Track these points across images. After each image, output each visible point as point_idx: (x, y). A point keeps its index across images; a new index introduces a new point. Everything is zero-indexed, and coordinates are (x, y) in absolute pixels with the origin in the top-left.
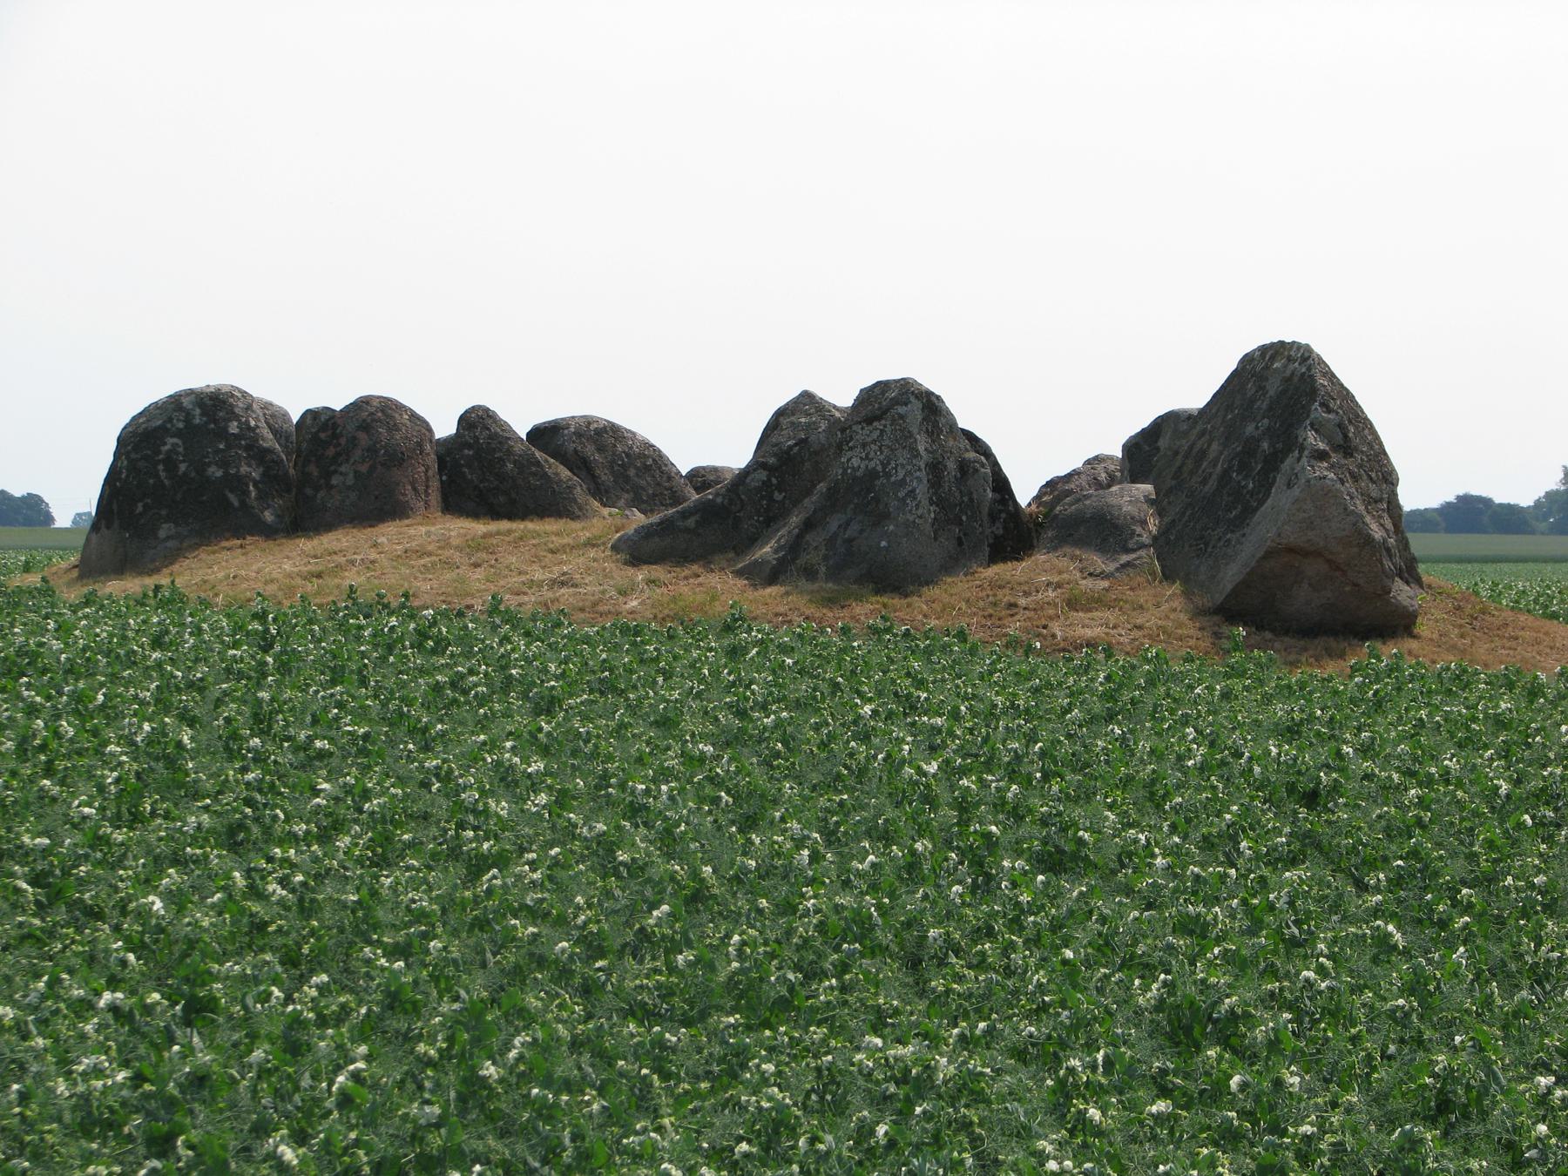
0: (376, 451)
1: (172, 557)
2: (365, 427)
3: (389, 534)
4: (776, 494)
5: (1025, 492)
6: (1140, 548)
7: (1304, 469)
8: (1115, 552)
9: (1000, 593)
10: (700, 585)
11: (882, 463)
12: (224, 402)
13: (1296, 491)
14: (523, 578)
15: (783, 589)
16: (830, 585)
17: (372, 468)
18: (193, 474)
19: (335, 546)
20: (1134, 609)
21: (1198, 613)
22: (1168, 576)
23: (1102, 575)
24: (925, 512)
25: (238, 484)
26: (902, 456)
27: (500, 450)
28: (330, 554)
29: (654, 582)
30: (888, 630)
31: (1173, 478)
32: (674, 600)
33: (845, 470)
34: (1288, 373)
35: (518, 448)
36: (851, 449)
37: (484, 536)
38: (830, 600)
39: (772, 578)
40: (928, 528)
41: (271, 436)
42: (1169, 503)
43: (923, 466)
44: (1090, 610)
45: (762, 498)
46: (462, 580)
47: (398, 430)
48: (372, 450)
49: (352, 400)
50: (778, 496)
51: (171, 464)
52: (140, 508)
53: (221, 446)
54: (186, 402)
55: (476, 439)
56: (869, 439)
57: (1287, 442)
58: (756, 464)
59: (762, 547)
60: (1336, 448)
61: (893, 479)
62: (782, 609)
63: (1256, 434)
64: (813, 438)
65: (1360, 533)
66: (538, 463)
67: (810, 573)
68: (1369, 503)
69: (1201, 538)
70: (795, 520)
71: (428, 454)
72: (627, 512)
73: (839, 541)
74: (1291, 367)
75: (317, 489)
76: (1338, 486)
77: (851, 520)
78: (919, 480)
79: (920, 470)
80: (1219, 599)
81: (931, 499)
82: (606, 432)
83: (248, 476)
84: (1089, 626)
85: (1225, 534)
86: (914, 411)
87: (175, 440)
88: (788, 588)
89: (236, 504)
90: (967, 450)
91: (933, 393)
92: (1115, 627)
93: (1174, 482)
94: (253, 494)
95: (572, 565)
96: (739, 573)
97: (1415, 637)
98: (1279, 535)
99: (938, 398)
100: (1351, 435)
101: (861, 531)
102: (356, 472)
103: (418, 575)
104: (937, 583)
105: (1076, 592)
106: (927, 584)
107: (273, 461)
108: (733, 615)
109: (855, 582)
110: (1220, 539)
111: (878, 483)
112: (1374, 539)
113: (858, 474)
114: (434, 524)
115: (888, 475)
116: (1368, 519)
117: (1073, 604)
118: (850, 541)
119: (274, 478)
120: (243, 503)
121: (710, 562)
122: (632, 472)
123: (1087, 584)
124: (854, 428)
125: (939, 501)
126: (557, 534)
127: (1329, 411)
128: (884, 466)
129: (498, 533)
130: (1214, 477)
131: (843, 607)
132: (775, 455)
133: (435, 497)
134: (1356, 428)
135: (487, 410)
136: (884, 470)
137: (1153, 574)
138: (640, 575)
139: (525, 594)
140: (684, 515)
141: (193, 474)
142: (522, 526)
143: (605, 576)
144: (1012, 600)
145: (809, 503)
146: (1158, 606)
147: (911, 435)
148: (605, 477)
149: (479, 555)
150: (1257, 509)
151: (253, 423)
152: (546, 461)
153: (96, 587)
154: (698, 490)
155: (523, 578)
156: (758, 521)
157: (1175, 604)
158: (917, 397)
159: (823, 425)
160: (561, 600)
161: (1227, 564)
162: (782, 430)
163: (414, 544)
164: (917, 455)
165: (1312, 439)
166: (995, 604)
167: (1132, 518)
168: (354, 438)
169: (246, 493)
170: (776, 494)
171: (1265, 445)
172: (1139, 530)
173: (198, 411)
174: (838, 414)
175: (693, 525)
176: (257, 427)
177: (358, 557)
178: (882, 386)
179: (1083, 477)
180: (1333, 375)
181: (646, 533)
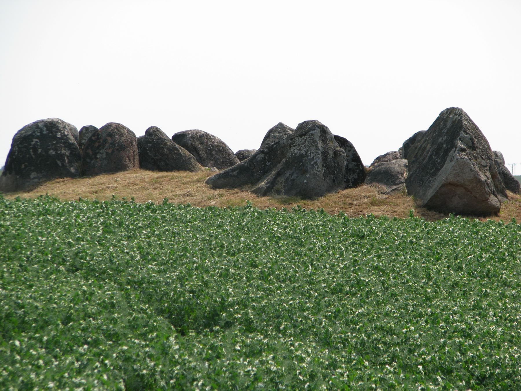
0: (115, 145)
1: (37, 185)
2: (110, 135)
3: (120, 176)
4: (267, 162)
5: (367, 161)
6: (400, 183)
7: (456, 155)
8: (391, 185)
9: (347, 199)
10: (238, 196)
11: (305, 152)
12: (55, 125)
13: (453, 163)
14: (173, 194)
15: (268, 198)
16: (285, 196)
17: (113, 151)
18: (44, 153)
19: (100, 181)
20: (395, 206)
21: (418, 207)
22: (409, 194)
23: (386, 193)
24: (320, 169)
25: (61, 157)
26: (313, 149)
27: (162, 144)
28: (99, 184)
29: (221, 195)
30: (299, 210)
31: (414, 157)
32: (228, 201)
33: (292, 154)
34: (454, 119)
35: (169, 143)
36: (294, 146)
37: (157, 178)
38: (285, 201)
39: (265, 194)
40: (321, 175)
41: (73, 138)
42: (412, 167)
43: (320, 153)
44: (379, 206)
45: (262, 164)
46: (150, 194)
47: (123, 136)
48: (113, 144)
49: (104, 124)
50: (268, 163)
51: (35, 149)
52: (23, 166)
53: (54, 142)
54: (40, 125)
55: (153, 139)
56: (301, 143)
57: (452, 145)
58: (260, 151)
59: (261, 182)
60: (469, 147)
61: (309, 158)
62: (267, 205)
63: (442, 141)
64: (281, 142)
65: (476, 178)
66: (177, 149)
67: (278, 192)
68: (481, 167)
69: (421, 180)
70: (274, 172)
71: (134, 146)
72: (212, 169)
73: (289, 180)
74: (456, 117)
75: (91, 159)
76: (469, 161)
77: (294, 172)
78: (318, 158)
79: (319, 154)
80: (426, 202)
81: (323, 165)
82: (204, 136)
83: (65, 154)
84: (378, 211)
85: (429, 178)
86: (317, 133)
87: (37, 140)
88: (270, 197)
89: (60, 165)
90: (337, 147)
91: (324, 126)
92: (387, 212)
93: (414, 159)
94: (67, 161)
95: (191, 188)
96: (253, 192)
97: (499, 216)
98: (447, 179)
99: (326, 127)
100: (475, 142)
101: (297, 177)
102: (106, 153)
103: (133, 192)
104: (324, 196)
105: (375, 199)
106: (321, 196)
107: (74, 148)
108: (247, 205)
109: (294, 195)
110: (427, 180)
111: (304, 159)
112: (482, 181)
113: (297, 155)
114: (137, 173)
115: (307, 156)
116: (480, 173)
117: (373, 203)
118: (293, 180)
119: (75, 155)
120: (63, 165)
121: (243, 188)
122: (214, 152)
123: (380, 196)
124: (295, 138)
125: (326, 166)
126: (186, 177)
127: (467, 134)
128: (306, 152)
129: (163, 177)
130: (427, 157)
131: (289, 204)
132: (267, 148)
133: (137, 162)
134: (478, 140)
135: (157, 128)
136: (306, 154)
137: (404, 193)
138: (216, 193)
139: (174, 199)
140: (233, 170)
141: (44, 153)
142: (172, 174)
143: (203, 193)
144: (351, 202)
145: (279, 166)
146: (404, 204)
147: (316, 142)
148: (203, 155)
149: (156, 185)
150: (440, 170)
151: (66, 133)
152: (180, 148)
153: (19, 195)
154: (240, 159)
155: (173, 194)
156: (260, 173)
157: (410, 204)
158: (318, 127)
159: (285, 137)
160: (187, 201)
161: (429, 189)
162: (270, 138)
163: (131, 181)
164: (318, 149)
165: (460, 144)
166: (345, 204)
167: (398, 172)
168: (106, 139)
169: (64, 160)
170: (267, 162)
171: (445, 146)
172: (400, 177)
173: (45, 129)
174: (291, 133)
175: (236, 174)
176: (68, 135)
177: (110, 186)
178: (306, 123)
179: (391, 156)
180: (471, 120)
181: (219, 177)
